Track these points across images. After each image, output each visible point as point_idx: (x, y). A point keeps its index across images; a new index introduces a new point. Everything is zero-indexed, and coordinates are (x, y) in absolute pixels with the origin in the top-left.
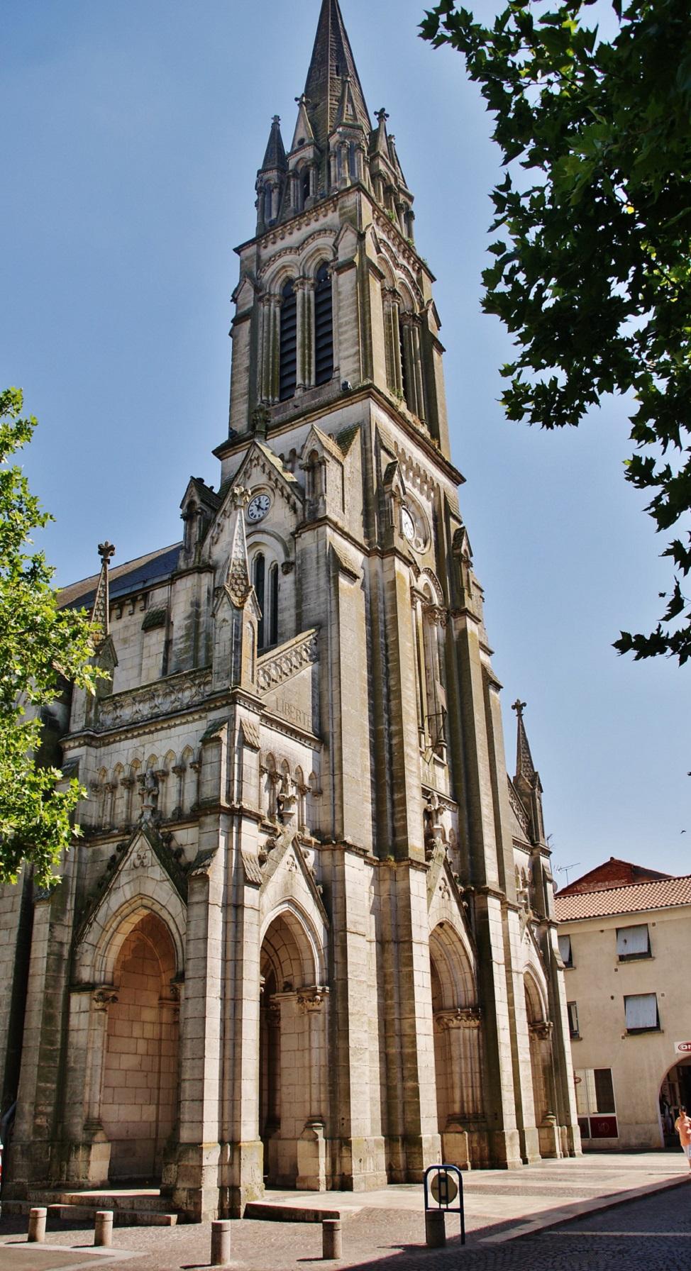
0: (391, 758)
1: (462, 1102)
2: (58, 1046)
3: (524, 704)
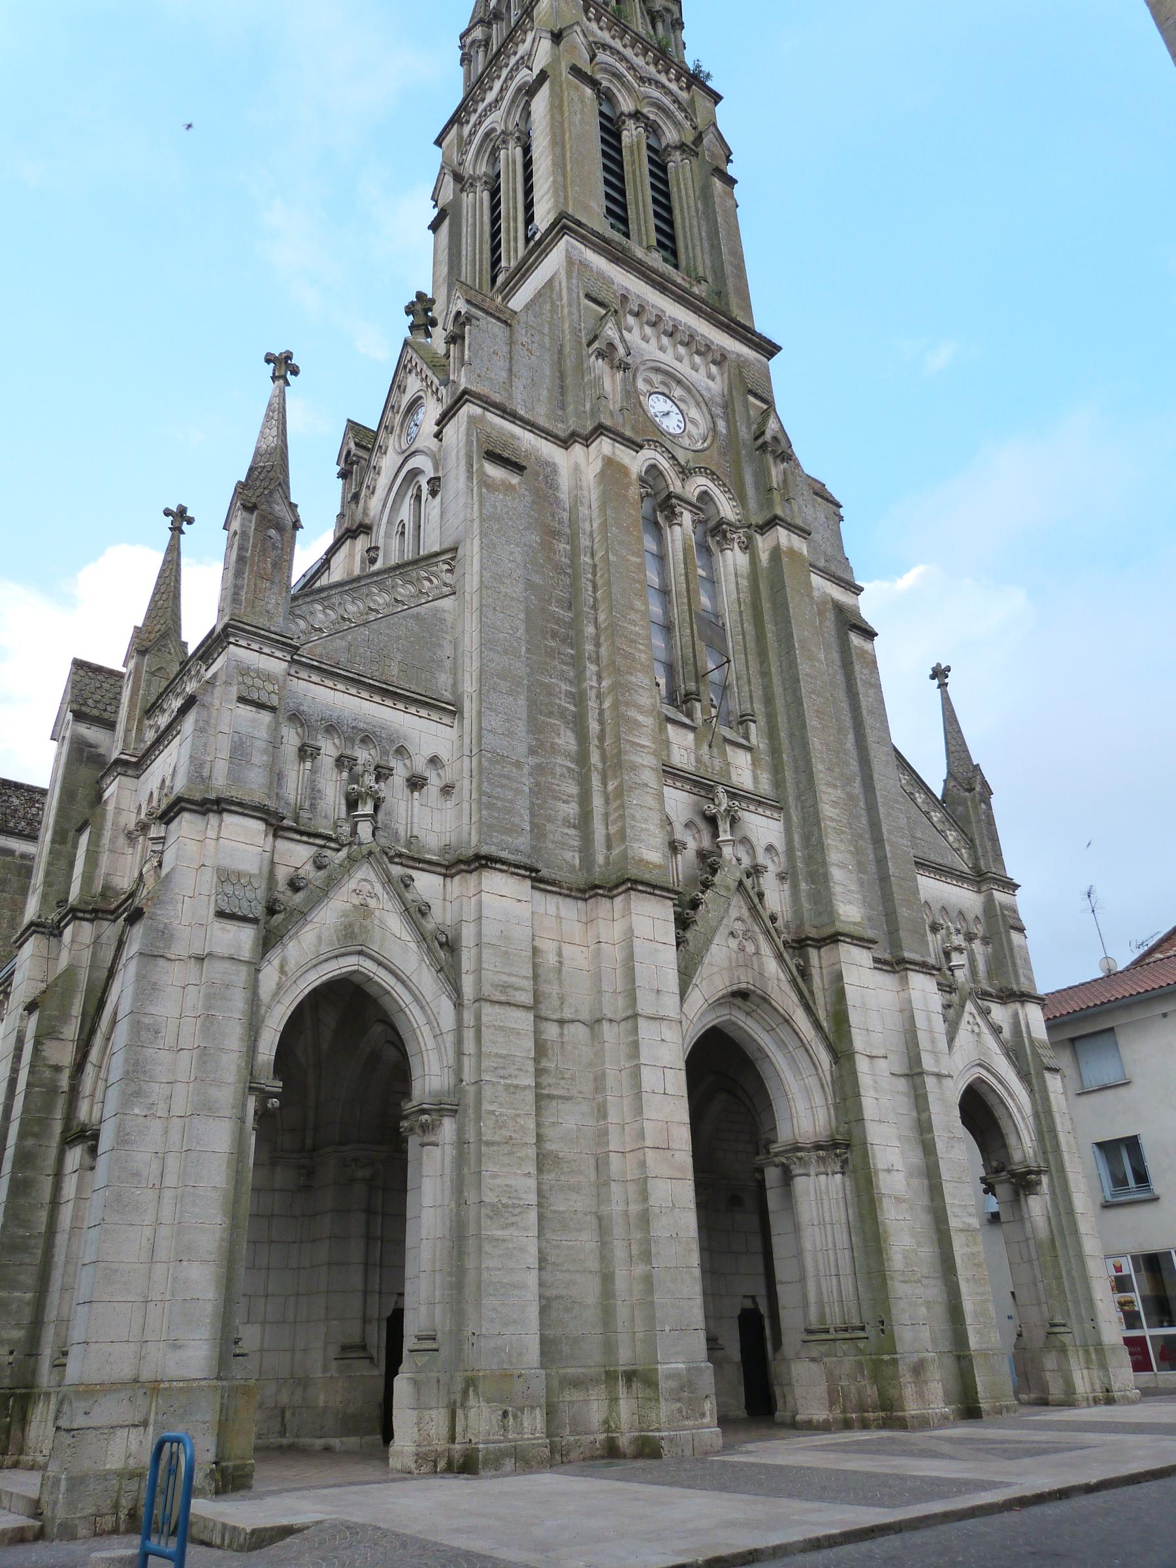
0: (603, 731)
1: (821, 1303)
3: (948, 669)
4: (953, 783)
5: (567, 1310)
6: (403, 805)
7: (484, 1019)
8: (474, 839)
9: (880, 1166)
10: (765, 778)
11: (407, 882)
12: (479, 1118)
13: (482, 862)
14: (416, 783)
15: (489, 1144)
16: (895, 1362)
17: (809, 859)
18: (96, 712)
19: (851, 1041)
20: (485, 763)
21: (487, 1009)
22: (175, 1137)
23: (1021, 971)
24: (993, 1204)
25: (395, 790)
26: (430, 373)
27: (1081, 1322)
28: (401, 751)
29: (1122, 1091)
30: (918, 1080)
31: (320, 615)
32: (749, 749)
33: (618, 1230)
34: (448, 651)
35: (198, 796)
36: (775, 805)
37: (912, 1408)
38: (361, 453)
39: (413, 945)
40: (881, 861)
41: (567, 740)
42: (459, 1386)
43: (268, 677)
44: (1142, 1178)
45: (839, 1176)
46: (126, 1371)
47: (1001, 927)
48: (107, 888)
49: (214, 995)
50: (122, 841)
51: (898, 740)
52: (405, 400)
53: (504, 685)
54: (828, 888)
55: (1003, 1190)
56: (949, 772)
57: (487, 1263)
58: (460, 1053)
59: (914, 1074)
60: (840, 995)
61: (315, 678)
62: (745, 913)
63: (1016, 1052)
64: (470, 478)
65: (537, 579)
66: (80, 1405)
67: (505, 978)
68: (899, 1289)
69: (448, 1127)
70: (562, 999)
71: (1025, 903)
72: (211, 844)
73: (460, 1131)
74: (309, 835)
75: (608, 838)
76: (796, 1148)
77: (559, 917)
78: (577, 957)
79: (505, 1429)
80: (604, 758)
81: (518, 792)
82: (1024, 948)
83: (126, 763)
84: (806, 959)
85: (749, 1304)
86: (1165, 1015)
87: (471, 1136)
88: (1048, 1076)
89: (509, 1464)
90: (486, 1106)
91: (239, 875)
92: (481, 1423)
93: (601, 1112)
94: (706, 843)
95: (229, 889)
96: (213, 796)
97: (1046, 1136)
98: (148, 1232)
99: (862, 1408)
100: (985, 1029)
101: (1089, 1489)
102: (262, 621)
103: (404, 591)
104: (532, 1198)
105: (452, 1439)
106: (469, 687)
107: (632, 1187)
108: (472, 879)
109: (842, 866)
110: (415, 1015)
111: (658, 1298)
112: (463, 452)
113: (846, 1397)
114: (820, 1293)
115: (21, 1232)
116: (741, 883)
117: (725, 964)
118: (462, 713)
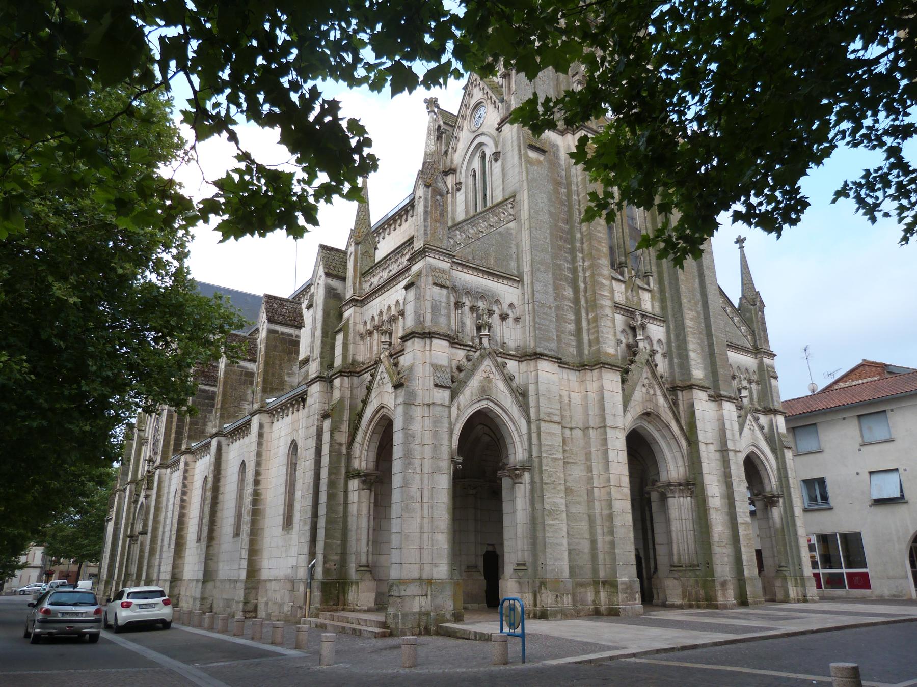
0: (586, 287)
1: (679, 554)
2: (342, 514)
3: (745, 239)
4: (744, 301)
5: (577, 555)
6: (498, 328)
7: (542, 429)
8: (532, 345)
9: (709, 494)
10: (657, 305)
11: (504, 365)
12: (541, 472)
13: (537, 356)
14: (504, 317)
15: (546, 484)
16: (714, 581)
17: (679, 347)
18: (335, 273)
19: (697, 436)
20: (536, 307)
21: (543, 425)
22: (426, 482)
23: (775, 399)
24: (753, 508)
25: (495, 320)
26: (489, 92)
27: (794, 566)
28: (497, 302)
29: (818, 455)
30: (725, 454)
31: (459, 236)
32: (649, 291)
33: (598, 522)
34: (514, 250)
35: (420, 331)
36: (661, 319)
37: (721, 600)
38: (447, 128)
39: (509, 395)
40: (711, 345)
41: (569, 292)
42: (538, 585)
43: (443, 271)
44: (825, 498)
45: (689, 498)
46: (415, 574)
47: (766, 376)
48: (353, 361)
49: (437, 422)
50: (358, 338)
51: (720, 283)
52: (473, 102)
53: (542, 268)
54: (688, 362)
55: (759, 504)
56: (743, 295)
57: (548, 535)
58: (530, 444)
59: (724, 450)
60: (693, 414)
61: (460, 269)
62: (650, 375)
63: (771, 439)
64: (520, 158)
65: (553, 210)
66: (402, 588)
67: (549, 410)
68: (716, 549)
69: (527, 476)
70: (571, 418)
71: (779, 365)
72: (428, 353)
73: (532, 478)
74: (464, 345)
75: (590, 341)
76: (670, 485)
77: (568, 379)
78: (576, 398)
79: (557, 602)
80: (587, 302)
81: (551, 321)
82: (777, 387)
83: (356, 300)
84: (676, 396)
85: (490, 548)
86: (844, 419)
87: (537, 480)
88: (786, 451)
89: (559, 616)
90: (544, 468)
91: (441, 366)
92: (547, 599)
93: (590, 469)
94: (631, 340)
95: (438, 374)
96: (427, 331)
97: (783, 480)
98: (419, 520)
99: (698, 600)
100: (756, 428)
101: (813, 632)
102: (438, 244)
103: (493, 220)
104: (564, 507)
105: (535, 605)
106: (526, 269)
107: (603, 503)
108: (532, 363)
109: (695, 351)
110: (511, 427)
111: (617, 551)
112: (515, 143)
113: (690, 594)
114: (679, 550)
115: (333, 515)
116: (648, 361)
117: (641, 400)
118: (523, 282)
